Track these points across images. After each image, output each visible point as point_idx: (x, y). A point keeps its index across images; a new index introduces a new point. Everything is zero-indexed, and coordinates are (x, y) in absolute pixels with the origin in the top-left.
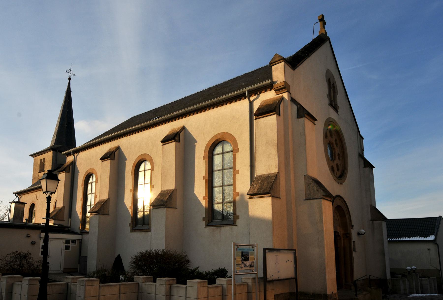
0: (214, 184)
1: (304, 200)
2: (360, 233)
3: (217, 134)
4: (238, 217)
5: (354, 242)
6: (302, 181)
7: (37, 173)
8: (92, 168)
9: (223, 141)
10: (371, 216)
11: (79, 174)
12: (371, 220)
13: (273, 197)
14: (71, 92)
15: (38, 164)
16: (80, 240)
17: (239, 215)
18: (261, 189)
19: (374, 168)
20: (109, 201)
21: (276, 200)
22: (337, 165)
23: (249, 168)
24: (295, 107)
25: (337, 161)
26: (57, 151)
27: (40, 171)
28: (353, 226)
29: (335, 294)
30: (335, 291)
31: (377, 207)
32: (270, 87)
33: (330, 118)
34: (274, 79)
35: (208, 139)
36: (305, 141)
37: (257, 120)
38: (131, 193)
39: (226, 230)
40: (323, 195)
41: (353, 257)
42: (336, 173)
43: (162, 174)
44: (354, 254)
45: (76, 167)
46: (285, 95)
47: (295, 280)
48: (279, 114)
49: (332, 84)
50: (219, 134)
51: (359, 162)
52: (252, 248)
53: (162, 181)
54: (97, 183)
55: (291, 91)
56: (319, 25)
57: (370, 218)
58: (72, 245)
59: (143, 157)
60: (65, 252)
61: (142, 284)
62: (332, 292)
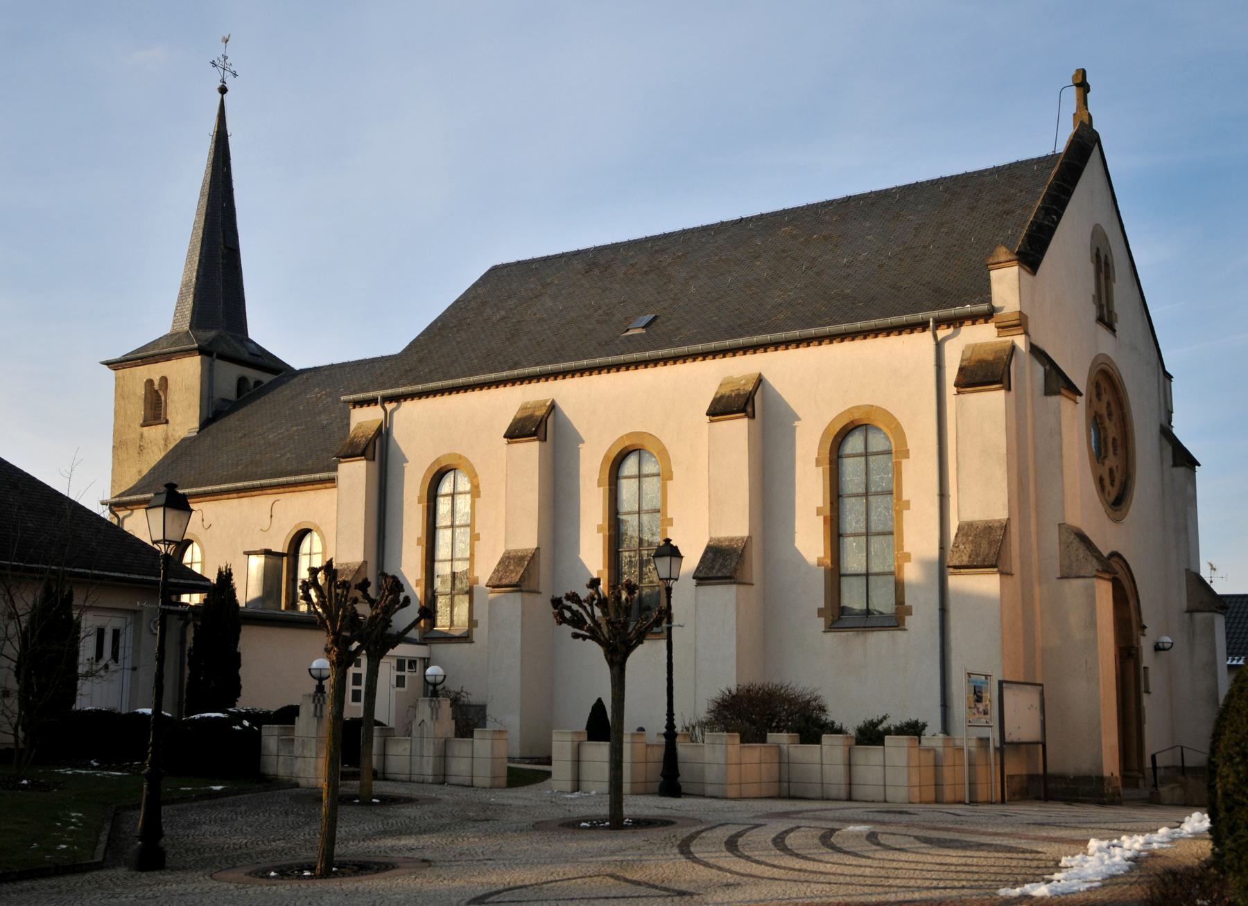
0: (842, 526)
1: (1058, 578)
2: (1161, 645)
3: (852, 408)
4: (909, 611)
5: (1146, 668)
6: (1053, 537)
7: (137, 426)
8: (456, 454)
9: (866, 425)
10: (1189, 600)
11: (405, 465)
12: (1187, 612)
13: (1002, 573)
14: (227, 136)
15: (135, 394)
16: (424, 659)
17: (911, 607)
18: (977, 555)
19: (1197, 467)
20: (539, 556)
21: (1005, 578)
22: (1111, 471)
23: (936, 499)
24: (1040, 370)
25: (1112, 461)
26: (215, 355)
27: (144, 421)
28: (1144, 627)
29: (1117, 778)
30: (1117, 773)
31: (1201, 574)
32: (988, 316)
33: (1099, 355)
34: (997, 302)
35: (828, 418)
36: (1061, 449)
37: (961, 396)
38: (601, 535)
39: (879, 640)
40: (1097, 570)
41: (1144, 708)
42: (1109, 493)
43: (709, 497)
44: (1146, 699)
45: (391, 446)
46: (1020, 341)
47: (1041, 746)
48: (1009, 389)
49: (1103, 259)
50: (858, 408)
51: (1161, 450)
52: (986, 679)
53: (709, 513)
54: (477, 499)
55: (1031, 331)
56: (1072, 93)
57: (1184, 605)
58: (410, 674)
59: (635, 441)
60: (397, 692)
61: (788, 748)
62: (1112, 774)
